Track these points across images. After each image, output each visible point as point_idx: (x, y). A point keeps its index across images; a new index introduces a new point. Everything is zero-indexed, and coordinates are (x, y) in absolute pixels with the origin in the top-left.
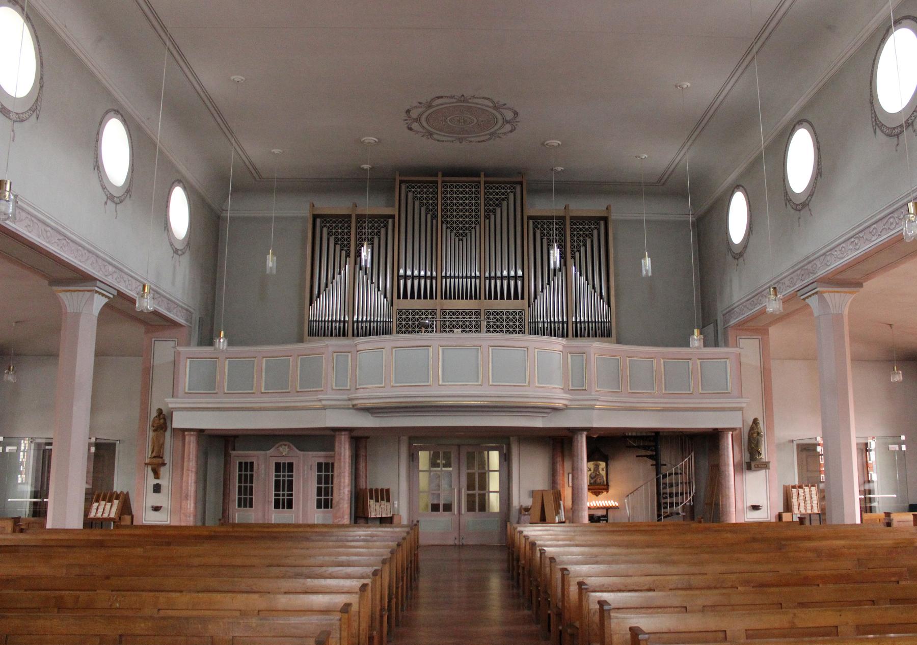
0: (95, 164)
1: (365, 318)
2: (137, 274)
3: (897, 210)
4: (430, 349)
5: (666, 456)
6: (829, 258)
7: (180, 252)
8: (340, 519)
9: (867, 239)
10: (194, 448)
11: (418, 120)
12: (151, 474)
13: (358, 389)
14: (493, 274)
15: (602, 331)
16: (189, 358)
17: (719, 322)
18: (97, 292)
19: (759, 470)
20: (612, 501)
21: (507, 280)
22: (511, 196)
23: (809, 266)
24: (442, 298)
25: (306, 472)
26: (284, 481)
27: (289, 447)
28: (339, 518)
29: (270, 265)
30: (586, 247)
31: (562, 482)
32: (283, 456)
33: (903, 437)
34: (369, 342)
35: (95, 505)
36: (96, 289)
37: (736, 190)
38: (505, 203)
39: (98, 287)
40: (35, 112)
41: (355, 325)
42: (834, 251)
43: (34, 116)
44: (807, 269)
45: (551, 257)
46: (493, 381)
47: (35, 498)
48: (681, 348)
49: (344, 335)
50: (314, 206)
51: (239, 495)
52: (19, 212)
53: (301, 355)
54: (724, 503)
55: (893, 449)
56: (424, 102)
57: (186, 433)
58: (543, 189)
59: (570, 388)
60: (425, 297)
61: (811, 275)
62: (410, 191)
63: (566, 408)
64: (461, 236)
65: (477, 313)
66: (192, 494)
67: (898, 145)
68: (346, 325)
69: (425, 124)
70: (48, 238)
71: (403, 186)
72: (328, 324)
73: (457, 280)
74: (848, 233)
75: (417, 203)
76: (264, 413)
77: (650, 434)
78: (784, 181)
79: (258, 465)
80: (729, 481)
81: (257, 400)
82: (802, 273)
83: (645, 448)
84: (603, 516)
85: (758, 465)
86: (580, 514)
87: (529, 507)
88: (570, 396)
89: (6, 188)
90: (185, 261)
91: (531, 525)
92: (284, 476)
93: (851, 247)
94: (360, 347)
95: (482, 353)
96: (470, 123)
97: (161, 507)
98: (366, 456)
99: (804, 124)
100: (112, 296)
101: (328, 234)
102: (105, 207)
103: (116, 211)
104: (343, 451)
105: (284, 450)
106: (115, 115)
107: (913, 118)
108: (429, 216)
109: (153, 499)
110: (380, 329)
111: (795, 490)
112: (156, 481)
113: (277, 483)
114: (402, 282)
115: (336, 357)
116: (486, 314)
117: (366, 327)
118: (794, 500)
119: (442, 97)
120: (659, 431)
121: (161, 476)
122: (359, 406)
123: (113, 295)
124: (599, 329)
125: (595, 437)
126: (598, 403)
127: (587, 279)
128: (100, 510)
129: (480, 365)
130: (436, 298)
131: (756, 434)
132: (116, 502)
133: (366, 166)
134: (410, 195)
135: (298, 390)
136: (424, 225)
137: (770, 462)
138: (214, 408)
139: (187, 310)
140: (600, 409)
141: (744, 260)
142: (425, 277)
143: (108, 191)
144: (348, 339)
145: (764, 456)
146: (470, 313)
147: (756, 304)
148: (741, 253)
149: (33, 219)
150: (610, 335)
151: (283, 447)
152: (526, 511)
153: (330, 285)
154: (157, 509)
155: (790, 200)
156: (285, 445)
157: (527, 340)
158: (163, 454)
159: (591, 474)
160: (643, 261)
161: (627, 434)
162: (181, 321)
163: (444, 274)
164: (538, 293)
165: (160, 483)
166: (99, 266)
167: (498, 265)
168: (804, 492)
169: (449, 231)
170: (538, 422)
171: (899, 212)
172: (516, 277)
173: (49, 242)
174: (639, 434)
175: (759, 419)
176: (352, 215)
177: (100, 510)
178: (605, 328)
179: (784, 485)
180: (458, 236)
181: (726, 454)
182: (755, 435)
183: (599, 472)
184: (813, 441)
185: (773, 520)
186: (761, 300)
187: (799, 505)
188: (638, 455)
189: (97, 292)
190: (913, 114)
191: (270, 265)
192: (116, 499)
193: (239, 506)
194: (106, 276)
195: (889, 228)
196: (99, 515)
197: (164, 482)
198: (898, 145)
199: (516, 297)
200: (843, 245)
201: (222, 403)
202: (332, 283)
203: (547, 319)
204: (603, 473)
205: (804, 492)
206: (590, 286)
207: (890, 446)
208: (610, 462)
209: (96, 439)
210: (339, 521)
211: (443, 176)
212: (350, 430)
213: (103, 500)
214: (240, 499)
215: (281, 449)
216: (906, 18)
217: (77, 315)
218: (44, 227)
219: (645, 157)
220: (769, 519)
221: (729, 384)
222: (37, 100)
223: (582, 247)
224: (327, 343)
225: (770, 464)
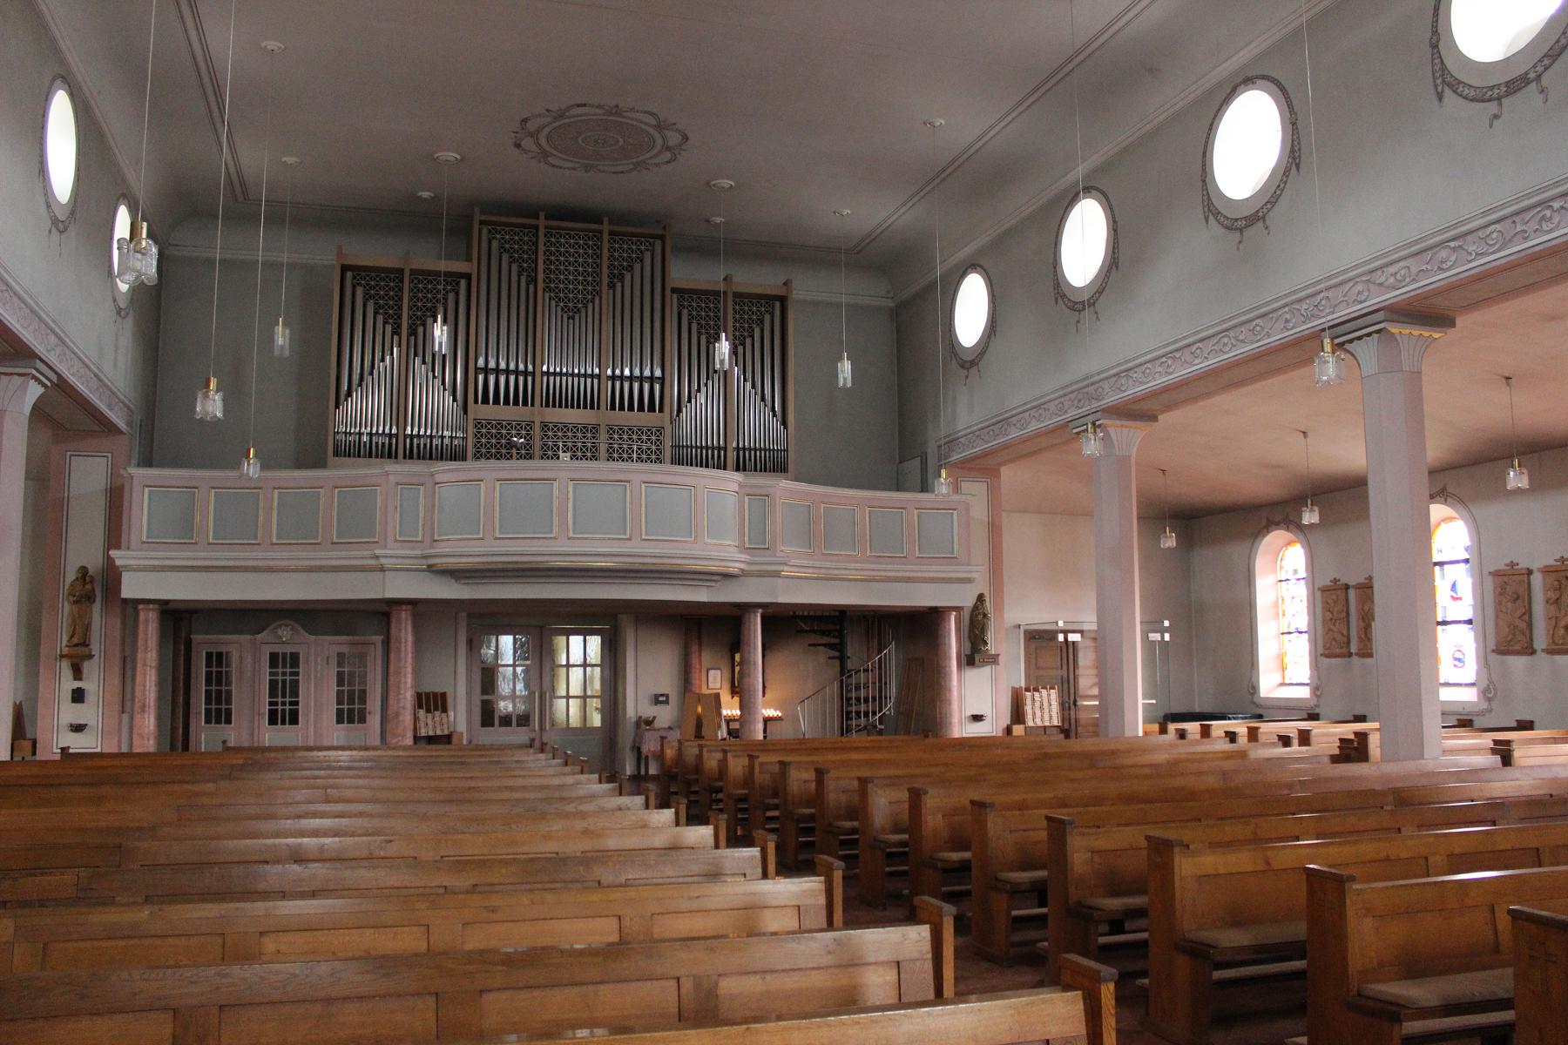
1: (381, 429)
2: (77, 347)
3: (1235, 327)
4: (556, 484)
5: (854, 649)
6: (1123, 381)
8: (400, 738)
9: (1185, 361)
10: (155, 632)
12: (67, 672)
15: (774, 463)
16: (214, 488)
17: (929, 456)
20: (772, 710)
23: (1091, 389)
25: (319, 667)
26: (284, 682)
28: (399, 736)
29: (280, 343)
30: (753, 339)
31: (697, 682)
32: (284, 643)
33: (1166, 623)
34: (456, 470)
36: (34, 372)
38: (637, 267)
41: (408, 440)
42: (1132, 372)
44: (1087, 393)
46: (646, 535)
53: (279, 488)
54: (943, 712)
55: (1153, 639)
56: (554, 110)
57: (141, 607)
58: (705, 248)
59: (747, 546)
60: (516, 403)
61: (1094, 401)
62: (493, 238)
63: (744, 574)
64: (571, 312)
65: (595, 429)
66: (152, 704)
67: (1240, 242)
69: (543, 141)
71: (485, 231)
74: (1154, 350)
75: (505, 257)
77: (833, 614)
78: (1055, 268)
80: (950, 681)
81: (261, 555)
82: (1080, 397)
83: (823, 633)
86: (752, 727)
87: (651, 719)
88: (748, 557)
89: (141, 234)
90: (129, 324)
92: (284, 674)
93: (1160, 369)
94: (439, 478)
95: (631, 491)
99: (1094, 192)
104: (403, 635)
105: (285, 633)
107: (1265, 210)
108: (523, 279)
109: (71, 713)
110: (447, 450)
111: (1030, 693)
112: (77, 684)
114: (481, 378)
115: (401, 491)
116: (476, 426)
117: (425, 445)
118: (1028, 708)
119: (584, 105)
120: (845, 609)
121: (84, 676)
122: (438, 567)
124: (770, 460)
126: (786, 568)
127: (753, 386)
130: (532, 405)
134: (495, 244)
135: (335, 540)
136: (516, 290)
137: (998, 655)
138: (199, 567)
139: (128, 408)
140: (788, 577)
141: (979, 371)
142: (517, 372)
144: (397, 463)
145: (992, 648)
146: (585, 428)
147: (998, 435)
148: (974, 360)
151: (283, 628)
152: (647, 726)
154: (78, 728)
155: (1063, 296)
156: (286, 626)
158: (89, 641)
160: (839, 365)
161: (797, 613)
162: (122, 425)
163: (481, 363)
164: (683, 405)
167: (636, 359)
168: (1041, 697)
169: (553, 303)
171: (1238, 330)
172: (652, 379)
174: (819, 614)
175: (985, 594)
179: (1013, 688)
181: (947, 642)
182: (980, 617)
184: (1053, 627)
185: (1000, 734)
186: (1006, 430)
187: (1034, 714)
188: (810, 642)
190: (1265, 205)
191: (280, 343)
193: (208, 721)
194: (48, 351)
195: (1221, 350)
197: (90, 685)
198: (1240, 242)
200: (1149, 365)
203: (437, 432)
205: (1041, 697)
206: (758, 398)
207: (1150, 635)
210: (399, 741)
211: (546, 218)
212: (413, 603)
214: (208, 712)
215: (280, 632)
216: (1264, 77)
220: (994, 734)
221: (955, 546)
224: (387, 469)
225: (1000, 657)
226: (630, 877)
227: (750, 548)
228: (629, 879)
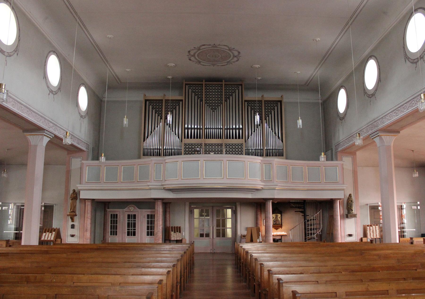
0: (44, 76)
1: (169, 147)
2: (63, 127)
3: (416, 97)
4: (200, 162)
5: (309, 212)
6: (384, 120)
7: (83, 117)
8: (157, 241)
9: (402, 111)
10: (90, 208)
11: (194, 56)
12: (70, 220)
13: (166, 180)
14: (228, 127)
15: (279, 154)
16: (88, 166)
17: (333, 149)
18: (45, 135)
19: (352, 218)
20: (284, 232)
21: (235, 130)
22: (237, 91)
23: (375, 123)
24: (205, 138)
25: (142, 219)
26: (132, 223)
27: (134, 207)
28: (157, 240)
29: (125, 123)
30: (272, 115)
31: (260, 223)
32: (131, 211)
33: (418, 203)
34: (171, 158)
35: (44, 234)
36: (45, 134)
37: (341, 88)
38: (234, 94)
39: (45, 133)
40: (16, 52)
41: (165, 150)
42: (386, 116)
43: (16, 54)
44: (374, 125)
45: (256, 119)
46: (228, 177)
47: (16, 231)
48: (315, 161)
49: (159, 155)
50: (145, 95)
51: (111, 229)
52: (9, 98)
53: (139, 165)
54: (336, 233)
55: (414, 208)
56: (197, 47)
57: (86, 201)
58: (252, 88)
59: (264, 180)
60: (197, 138)
61: (376, 127)
62: (190, 89)
63: (262, 189)
64: (213, 109)
65: (221, 145)
66: (89, 229)
67: (416, 67)
68: (161, 150)
69: (197, 58)
70: (22, 110)
71: (187, 86)
72: (152, 150)
73: (212, 130)
74: (393, 108)
75: (193, 94)
76: (122, 191)
77: (301, 201)
78: (363, 84)
79: (120, 215)
80: (338, 223)
81: (119, 185)
82: (372, 126)
83: (299, 208)
84: (280, 239)
85: (351, 216)
86: (269, 238)
87: (245, 235)
88: (264, 184)
89: (3, 87)
90: (86, 121)
91: (246, 243)
92: (132, 221)
93: (394, 114)
94: (167, 161)
95: (223, 164)
96: (218, 57)
97: (74, 235)
98: (170, 211)
99: (373, 57)
100: (52, 137)
101: (152, 108)
102: (49, 96)
103: (54, 98)
104: (159, 209)
105: (132, 209)
106: (53, 53)
107: (423, 55)
108: (199, 100)
109: (71, 231)
110: (176, 153)
111: (369, 227)
112: (73, 223)
113: (128, 224)
114: (186, 131)
115: (156, 166)
117: (170, 152)
118: (368, 232)
119: (205, 45)
120: (305, 200)
121: (75, 221)
122: (166, 188)
123: (52, 137)
124: (277, 153)
125: (276, 202)
126: (277, 187)
127: (272, 129)
128: (46, 237)
129: (222, 169)
130: (202, 138)
131: (350, 201)
132: (54, 233)
133: (170, 77)
134: (190, 90)
135: (138, 181)
136: (197, 105)
137: (357, 214)
138: (99, 189)
139: (87, 144)
140: (278, 190)
141: (345, 121)
142: (197, 129)
143: (50, 89)
144: (161, 157)
145: (354, 212)
146: (218, 145)
147: (350, 141)
148: (343, 117)
149: (15, 101)
150: (283, 155)
151: (131, 207)
152: (244, 237)
153: (153, 132)
154: (73, 236)
155: (366, 93)
156: (132, 206)
157: (244, 158)
158: (75, 210)
159: (274, 220)
160: (298, 121)
161: (290, 201)
162: (84, 149)
163: (206, 127)
164: (249, 136)
165: (74, 224)
166: (46, 123)
167: (231, 123)
168: (373, 228)
169: (208, 107)
170: (249, 196)
171: (417, 98)
172: (239, 129)
173: (23, 112)
174: (296, 201)
175: (352, 194)
176: (163, 100)
177: (46, 237)
178: (281, 152)
179: (363, 225)
180: (212, 110)
181: (336, 210)
182: (350, 202)
183: (278, 219)
184: (377, 205)
185: (358, 241)
186: (353, 139)
187: (370, 234)
188: (296, 211)
189: (45, 135)
190: (423, 53)
191: (125, 123)
192: (54, 231)
193: (111, 234)
194: (49, 128)
195: (412, 106)
196: (46, 239)
197: (76, 223)
198: (416, 67)
199: (239, 138)
200: (391, 114)
201: (103, 187)
202: (154, 131)
204: (280, 219)
205: (373, 228)
206: (274, 133)
207: (412, 207)
208: (283, 214)
209: (45, 203)
210: (157, 242)
211: (205, 82)
212: (162, 199)
213: (48, 232)
214: (111, 232)
215: (130, 208)
216: (420, 8)
217: (36, 146)
218: (20, 105)
219: (299, 73)
220: (356, 241)
221: (338, 178)
222: (17, 46)
223: (270, 115)
224: (151, 159)
225: (357, 215)
226: (109, 294)
227: (229, 179)
228: (109, 295)
